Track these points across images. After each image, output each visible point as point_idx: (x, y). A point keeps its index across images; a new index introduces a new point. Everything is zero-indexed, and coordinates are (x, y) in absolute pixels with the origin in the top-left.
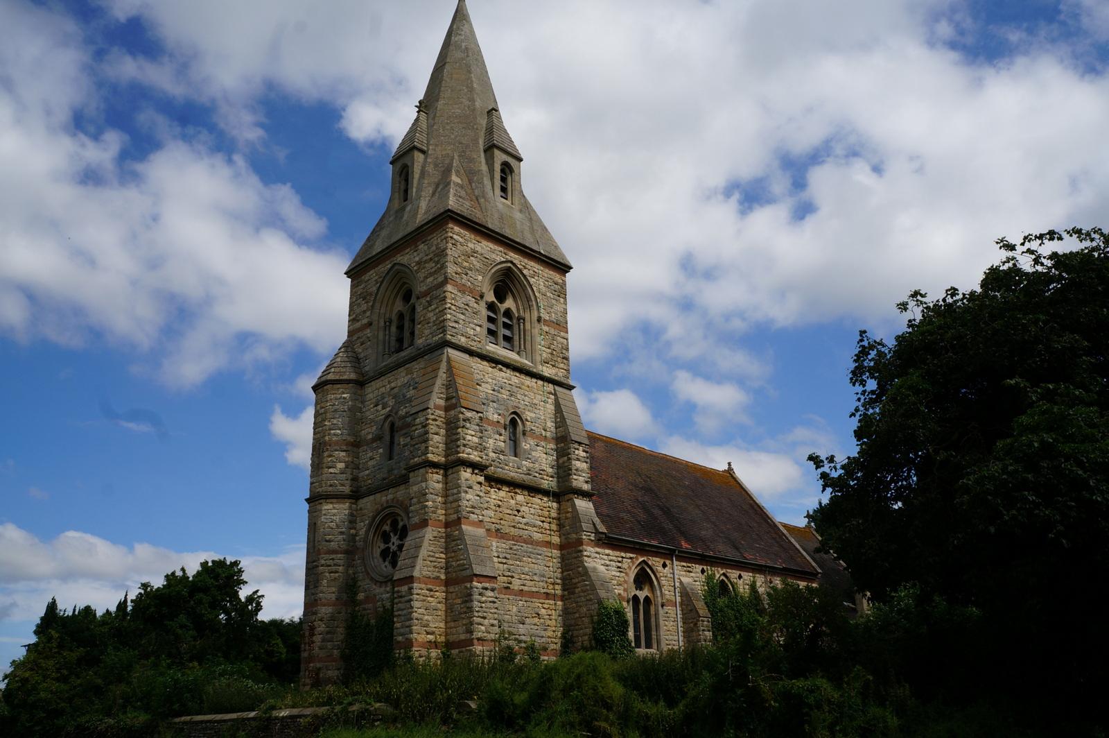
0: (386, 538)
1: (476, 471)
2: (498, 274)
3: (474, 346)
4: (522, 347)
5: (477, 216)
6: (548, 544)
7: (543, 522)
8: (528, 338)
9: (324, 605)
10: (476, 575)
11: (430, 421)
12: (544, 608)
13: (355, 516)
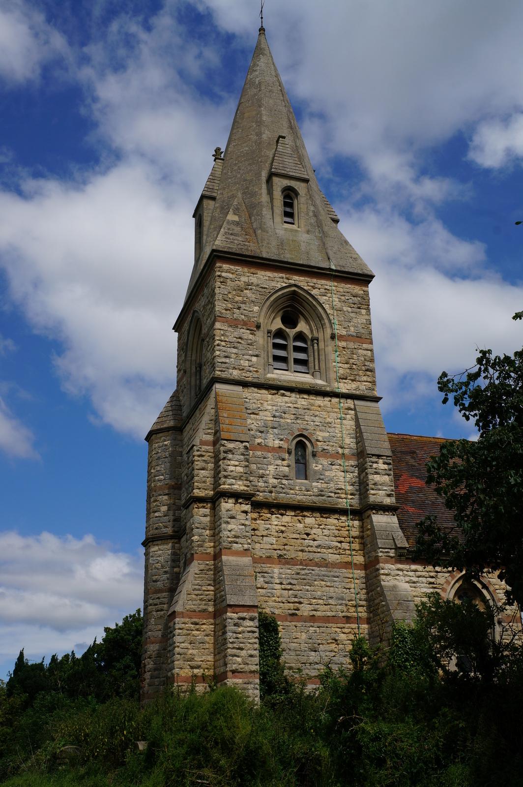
1: (240, 501)
2: (280, 301)
3: (250, 377)
4: (317, 368)
5: (252, 248)
6: (348, 565)
7: (341, 542)
8: (322, 357)
9: (153, 643)
10: (230, 606)
11: (196, 458)
12: (344, 633)
13: (179, 555)
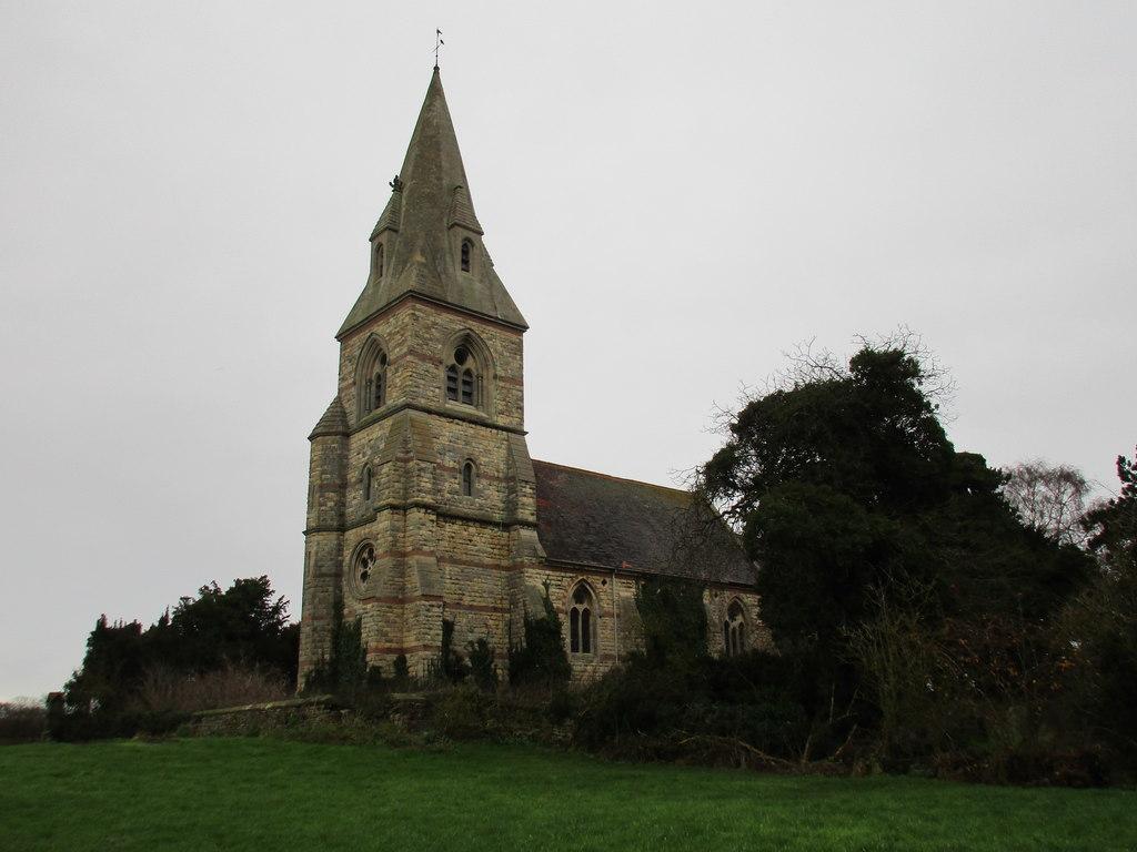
0: (365, 563)
3: (433, 405)
8: (485, 393)
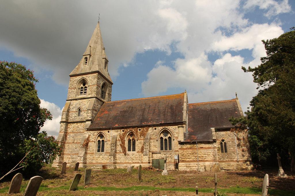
3: (73, 98)
